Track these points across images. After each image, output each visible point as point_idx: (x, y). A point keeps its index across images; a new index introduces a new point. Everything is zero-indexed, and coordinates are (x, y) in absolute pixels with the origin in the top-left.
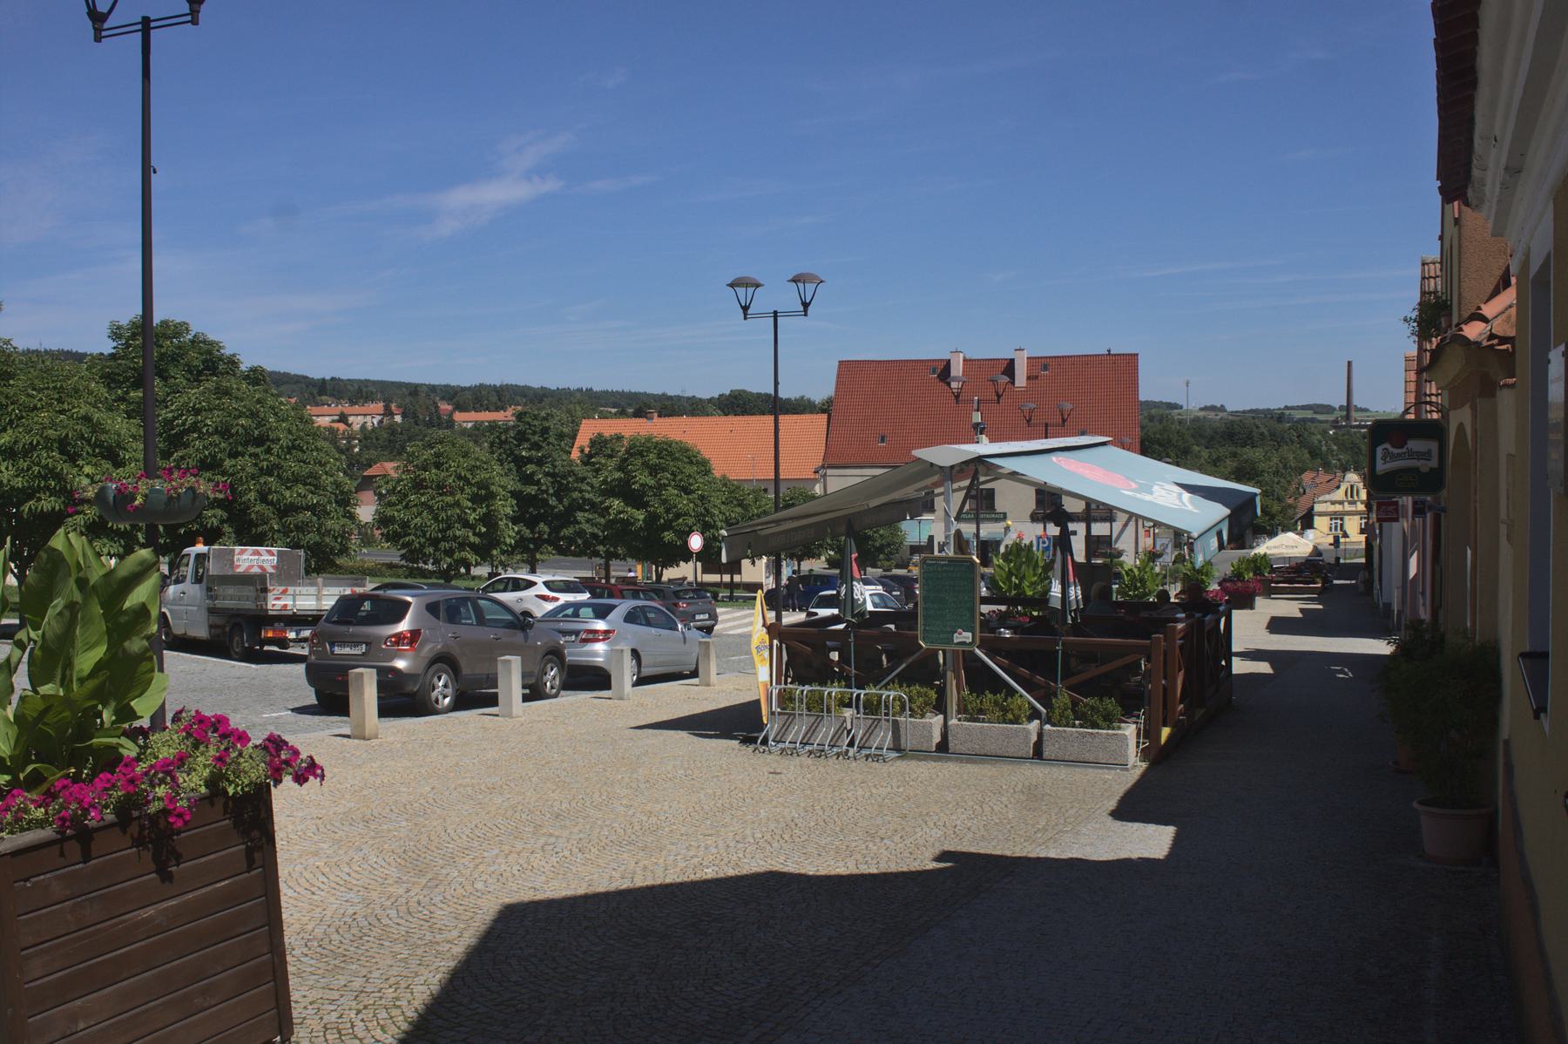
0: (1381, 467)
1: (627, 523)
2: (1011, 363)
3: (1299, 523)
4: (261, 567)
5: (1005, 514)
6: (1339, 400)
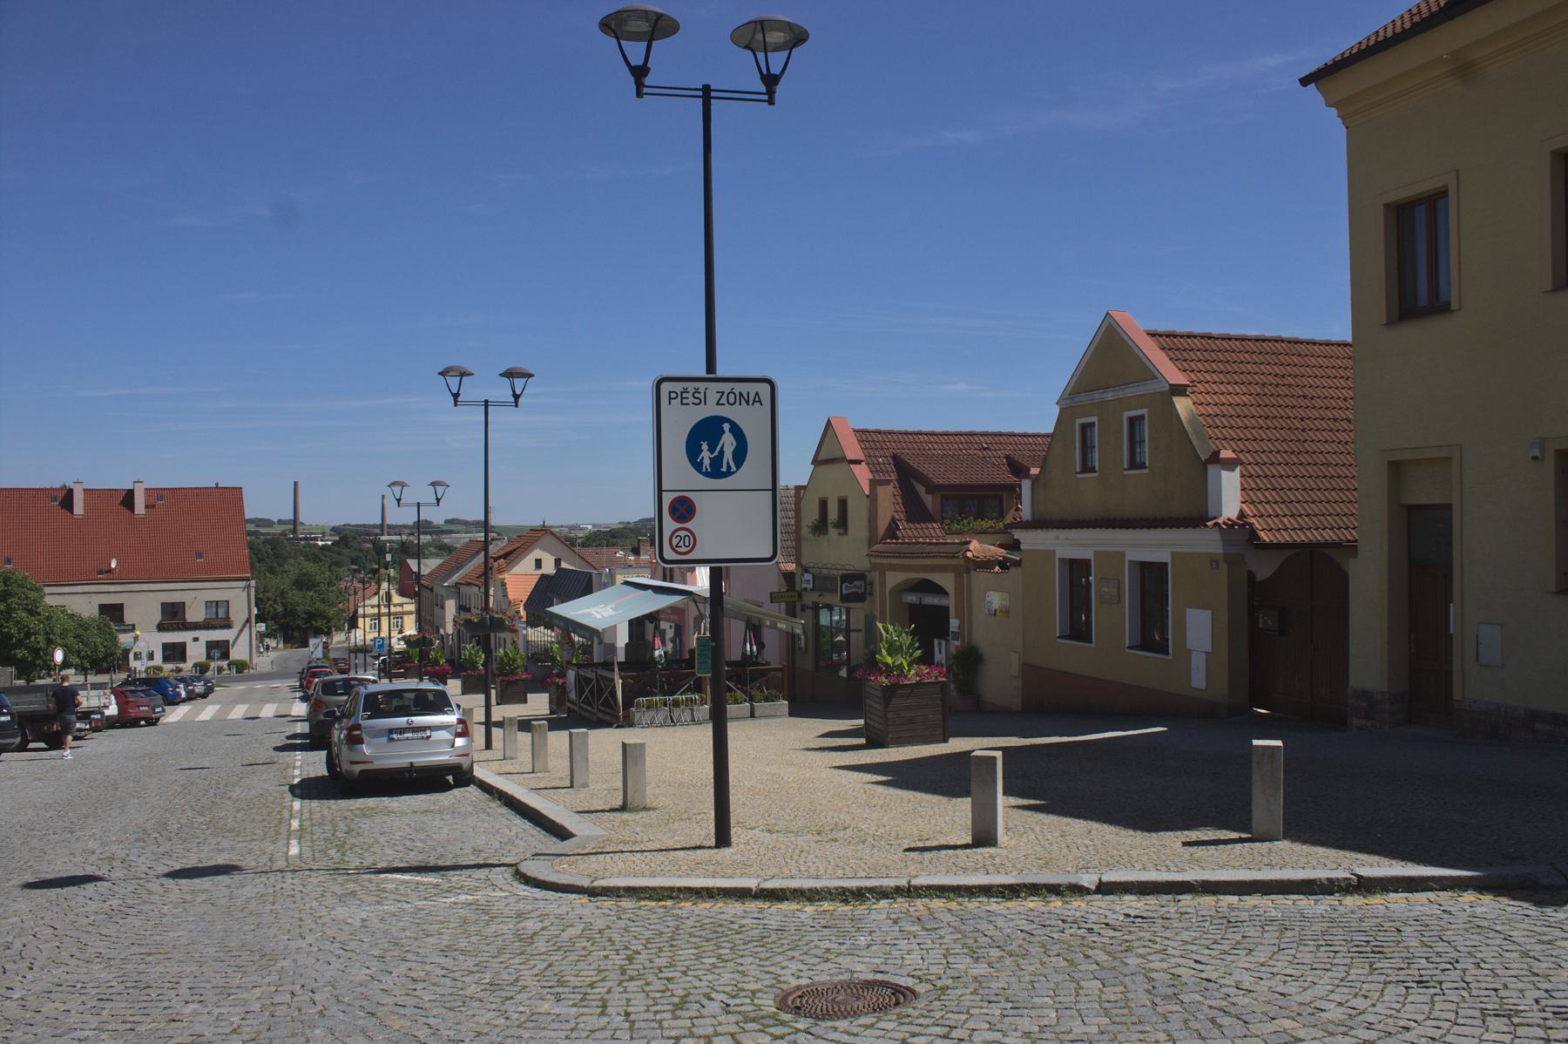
0: (844, 592)
2: (70, 492)
3: (346, 625)
5: (134, 625)
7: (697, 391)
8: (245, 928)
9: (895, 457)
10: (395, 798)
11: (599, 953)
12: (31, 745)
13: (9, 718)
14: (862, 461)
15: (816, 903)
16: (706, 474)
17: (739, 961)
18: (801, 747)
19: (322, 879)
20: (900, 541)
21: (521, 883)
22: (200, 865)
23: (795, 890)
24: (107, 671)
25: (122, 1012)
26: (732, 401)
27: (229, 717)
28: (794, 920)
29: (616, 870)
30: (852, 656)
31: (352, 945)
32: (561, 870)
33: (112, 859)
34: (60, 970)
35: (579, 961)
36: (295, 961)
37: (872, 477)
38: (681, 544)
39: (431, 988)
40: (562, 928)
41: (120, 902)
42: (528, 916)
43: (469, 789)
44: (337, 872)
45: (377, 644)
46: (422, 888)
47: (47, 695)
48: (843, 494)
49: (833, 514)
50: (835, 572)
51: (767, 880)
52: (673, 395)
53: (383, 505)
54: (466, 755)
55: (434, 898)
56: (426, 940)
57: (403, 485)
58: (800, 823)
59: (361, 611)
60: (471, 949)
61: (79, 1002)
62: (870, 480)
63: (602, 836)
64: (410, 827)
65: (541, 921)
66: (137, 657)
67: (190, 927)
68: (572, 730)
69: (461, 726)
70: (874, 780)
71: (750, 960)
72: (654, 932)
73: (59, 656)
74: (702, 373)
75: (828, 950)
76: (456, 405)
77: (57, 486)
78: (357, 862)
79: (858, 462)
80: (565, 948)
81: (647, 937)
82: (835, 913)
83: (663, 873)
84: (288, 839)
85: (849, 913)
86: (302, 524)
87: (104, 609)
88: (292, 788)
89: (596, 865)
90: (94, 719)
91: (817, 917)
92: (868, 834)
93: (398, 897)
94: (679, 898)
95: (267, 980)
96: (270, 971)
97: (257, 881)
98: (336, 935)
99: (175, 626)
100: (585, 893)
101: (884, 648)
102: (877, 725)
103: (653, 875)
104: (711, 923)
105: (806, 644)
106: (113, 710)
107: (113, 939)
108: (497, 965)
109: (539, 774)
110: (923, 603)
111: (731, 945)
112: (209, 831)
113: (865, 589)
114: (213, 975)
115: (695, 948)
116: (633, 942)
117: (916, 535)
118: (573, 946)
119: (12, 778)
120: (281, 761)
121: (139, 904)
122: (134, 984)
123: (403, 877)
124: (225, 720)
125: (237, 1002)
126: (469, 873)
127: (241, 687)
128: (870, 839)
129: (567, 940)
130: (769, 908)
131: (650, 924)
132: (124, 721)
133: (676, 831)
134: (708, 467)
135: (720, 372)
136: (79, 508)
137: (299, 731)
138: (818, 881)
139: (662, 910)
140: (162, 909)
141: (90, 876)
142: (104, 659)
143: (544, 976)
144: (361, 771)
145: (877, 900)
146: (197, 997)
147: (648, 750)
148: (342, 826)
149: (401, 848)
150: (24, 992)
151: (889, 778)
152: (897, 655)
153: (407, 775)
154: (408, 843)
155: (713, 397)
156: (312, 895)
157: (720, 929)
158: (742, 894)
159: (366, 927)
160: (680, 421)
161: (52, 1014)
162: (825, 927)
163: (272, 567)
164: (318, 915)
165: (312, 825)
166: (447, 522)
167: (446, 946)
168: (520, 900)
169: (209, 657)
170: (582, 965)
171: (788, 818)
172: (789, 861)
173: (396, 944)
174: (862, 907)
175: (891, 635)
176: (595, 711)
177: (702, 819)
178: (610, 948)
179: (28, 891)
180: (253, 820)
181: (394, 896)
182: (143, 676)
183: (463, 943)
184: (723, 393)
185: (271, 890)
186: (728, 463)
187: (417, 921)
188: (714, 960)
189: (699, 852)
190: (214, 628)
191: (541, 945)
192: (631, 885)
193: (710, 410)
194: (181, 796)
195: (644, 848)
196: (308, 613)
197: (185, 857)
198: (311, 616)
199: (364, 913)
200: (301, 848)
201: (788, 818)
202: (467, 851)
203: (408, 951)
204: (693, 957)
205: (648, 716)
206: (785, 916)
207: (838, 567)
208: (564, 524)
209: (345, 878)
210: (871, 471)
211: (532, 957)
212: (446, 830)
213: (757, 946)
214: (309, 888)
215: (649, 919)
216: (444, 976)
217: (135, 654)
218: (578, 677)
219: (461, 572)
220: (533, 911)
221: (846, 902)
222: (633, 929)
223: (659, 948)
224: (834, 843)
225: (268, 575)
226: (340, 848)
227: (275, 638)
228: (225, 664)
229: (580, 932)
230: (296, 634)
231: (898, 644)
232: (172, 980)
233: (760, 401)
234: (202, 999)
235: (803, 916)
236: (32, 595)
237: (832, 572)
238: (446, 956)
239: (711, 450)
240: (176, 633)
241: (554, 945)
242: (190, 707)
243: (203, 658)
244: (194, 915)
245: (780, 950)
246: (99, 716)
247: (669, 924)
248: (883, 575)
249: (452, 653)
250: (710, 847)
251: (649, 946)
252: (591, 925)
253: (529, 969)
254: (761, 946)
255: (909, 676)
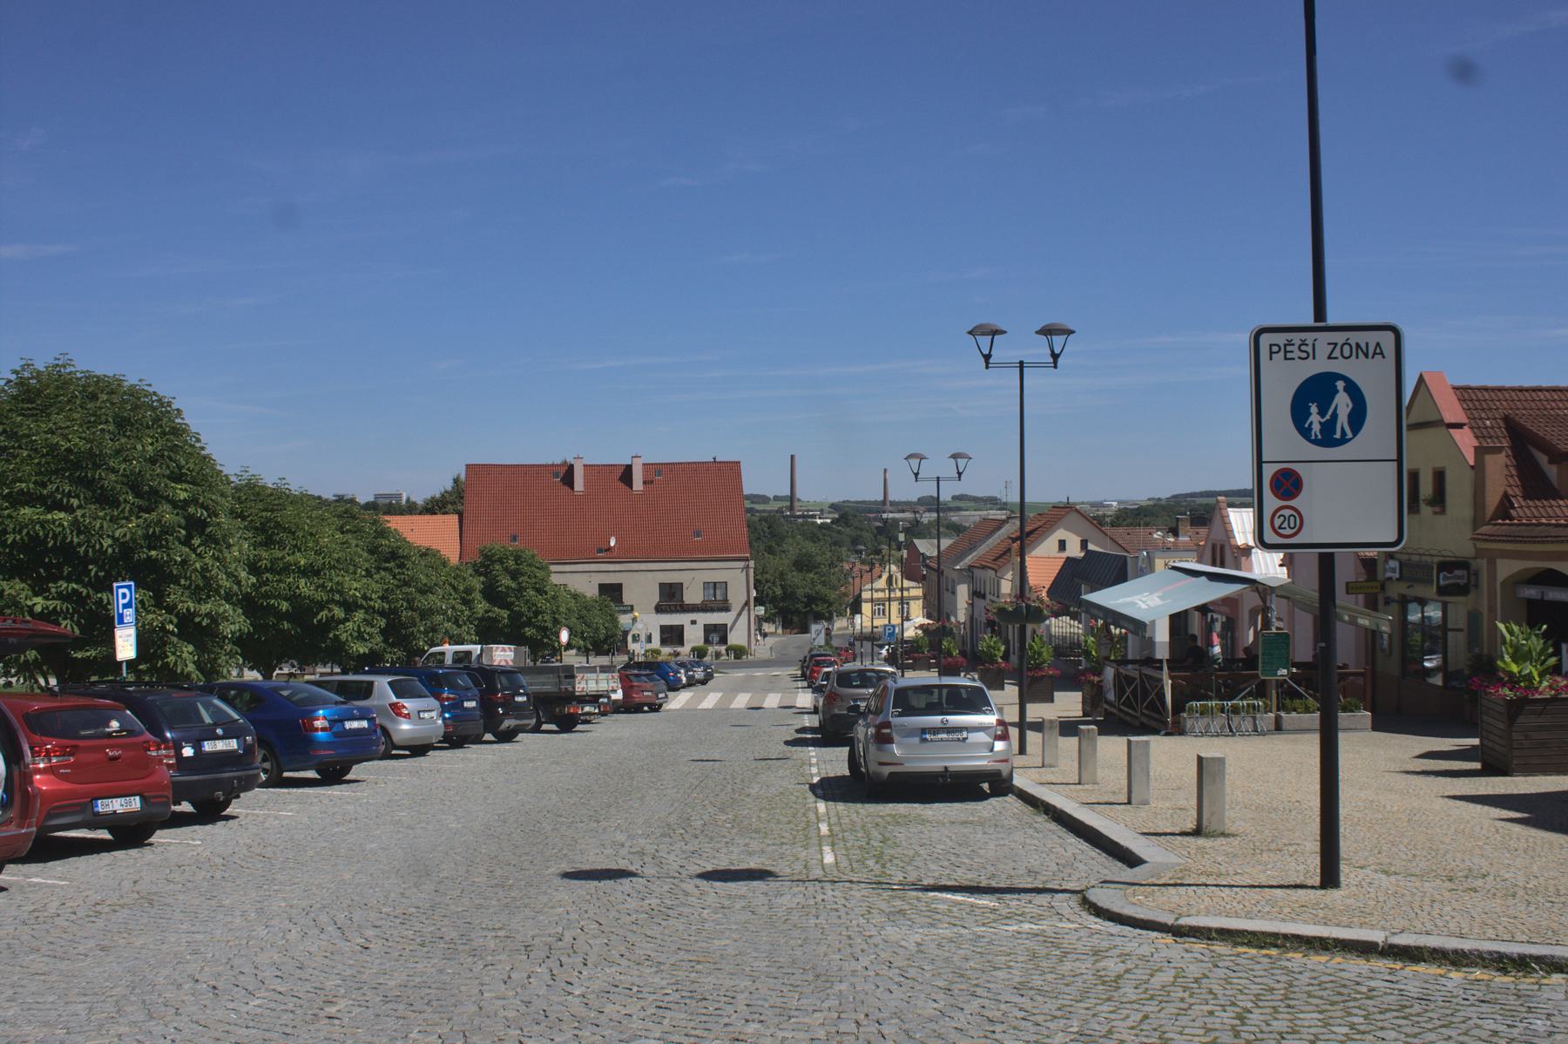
0: (1442, 582)
1: (496, 620)
4: (506, 661)
5: (632, 606)
6: (881, 498)
7: (1304, 343)
8: (792, 942)
9: (1506, 419)
10: (927, 806)
11: (1202, 1007)
12: (545, 727)
13: (525, 699)
14: (1465, 424)
15: (1464, 969)
16: (1316, 442)
17: (1379, 1034)
18: (1397, 770)
19: (864, 892)
20: (1516, 521)
21: (1091, 914)
22: (732, 868)
23: (1435, 951)
24: (606, 653)
25: (683, 1023)
26: (1347, 353)
27: (732, 706)
28: (1438, 987)
29: (1202, 906)
30: (1449, 660)
31: (912, 973)
32: (1138, 902)
33: (642, 853)
34: (613, 969)
35: (1178, 1015)
36: (853, 985)
37: (1477, 444)
38: (1285, 525)
39: (1012, 1031)
40: (1149, 972)
41: (658, 901)
42: (1107, 954)
43: (1006, 798)
44: (879, 886)
45: (887, 632)
46: (978, 912)
47: (559, 677)
48: (1438, 465)
49: (1426, 489)
50: (1429, 559)
51: (1394, 934)
52: (1275, 349)
53: (885, 480)
54: (1006, 761)
55: (994, 925)
56: (994, 973)
57: (922, 458)
58: (1423, 865)
59: (866, 595)
60: (1049, 989)
61: (639, 1006)
62: (1476, 448)
63: (1179, 864)
64: (951, 840)
65: (1123, 962)
66: (636, 639)
67: (735, 936)
68: (1132, 738)
69: (1000, 728)
70: (1505, 817)
71: (1393, 1034)
72: (1261, 986)
73: (564, 636)
74: (1309, 320)
75: (1495, 1033)
76: (987, 367)
77: (558, 461)
78: (899, 877)
79: (1459, 426)
80: (1160, 998)
81: (1256, 992)
82: (1492, 985)
83: (1260, 915)
84: (820, 845)
85: (1512, 987)
86: (799, 500)
87: (604, 588)
88: (813, 787)
89: (1176, 899)
90: (603, 703)
91: (1468, 987)
92: (1516, 885)
93: (953, 921)
94: (1285, 946)
95: (826, 1005)
96: (828, 995)
97: (796, 890)
98: (892, 960)
99: (673, 608)
100: (1168, 932)
101: (1508, 654)
102: (1497, 748)
103: (1249, 916)
104: (1332, 982)
105: (1390, 644)
106: (619, 695)
107: (659, 942)
108: (1084, 1011)
109: (1086, 786)
110: (1546, 598)
111: (1364, 1013)
112: (735, 831)
113: (1469, 580)
114: (768, 993)
115: (1319, 1012)
116: (1240, 997)
117: (1536, 514)
118: (1168, 995)
119: (531, 760)
120: (795, 757)
121: (678, 906)
122: (689, 994)
123: (954, 897)
124: (728, 709)
125: (800, 1026)
126: (1028, 898)
127: (740, 674)
128: (1521, 893)
129: (1159, 987)
130: (1401, 969)
131: (1255, 977)
132: (629, 707)
133: (1266, 864)
134: (1318, 433)
135: (1332, 319)
136: (579, 484)
137: (808, 725)
138: (1463, 940)
139: (1266, 960)
140: (701, 913)
141: (624, 871)
142: (605, 642)
143: (1142, 1030)
144: (890, 773)
145: (1547, 972)
146: (758, 1015)
147: (1229, 769)
148: (875, 833)
149: (946, 864)
150: (583, 989)
151: (1526, 815)
152: (1525, 662)
153: (941, 780)
154: (953, 858)
155: (1323, 350)
156: (857, 910)
157: (1345, 991)
158: (1365, 949)
159: (922, 952)
160: (1284, 380)
161: (615, 1016)
162: (1483, 1001)
163: (770, 547)
164: (868, 933)
165: (844, 831)
166: (955, 498)
167: (1020, 983)
168: (1092, 934)
169: (707, 641)
170: (1183, 1021)
171: (1405, 857)
172: (1419, 912)
173: (962, 976)
174: (1528, 980)
175: (1517, 638)
176: (1138, 714)
177: (1296, 851)
178: (1212, 1002)
179: (567, 880)
180: (779, 822)
181: (948, 919)
182: (641, 659)
183: (1037, 982)
184: (1336, 344)
185: (812, 902)
186: (1342, 428)
187: (979, 950)
188: (1345, 1030)
189: (1301, 892)
190: (712, 610)
191: (1129, 991)
192: (1225, 926)
193: (1320, 365)
194: (698, 790)
195: (1232, 883)
196: (808, 596)
197: (714, 857)
198: (811, 599)
199: (917, 936)
200: (836, 856)
201: (1405, 857)
202: (1021, 872)
203: (977, 985)
204: (1320, 1024)
205: (1200, 724)
206: (1426, 982)
207: (1432, 552)
208: (1085, 501)
209: (890, 893)
210: (1477, 437)
211: (1122, 1006)
212: (992, 846)
213: (1397, 1017)
214: (853, 902)
215: (1252, 970)
216: (1023, 1019)
217: (634, 636)
218: (1117, 675)
219: (974, 554)
220: (1110, 948)
221: (1504, 971)
222: (1235, 981)
223: (1274, 1007)
224: (1473, 894)
225: (766, 555)
226: (879, 858)
227: (774, 622)
228: (723, 649)
229: (1172, 979)
230: (795, 619)
231: (1526, 648)
232: (728, 993)
233: (1382, 353)
234: (762, 1018)
235: (1450, 985)
236: (540, 574)
237: (1424, 558)
238: (1022, 995)
239: (1322, 413)
240: (674, 615)
241: (1145, 993)
242: (692, 694)
243: (701, 643)
244: (736, 923)
245: (1430, 1026)
246: (606, 700)
247: (1278, 978)
248: (1492, 564)
249: (964, 643)
250: (1313, 887)
251: (1261, 1004)
252: (1184, 971)
253: (1122, 1020)
254: (1404, 1018)
255: (1541, 689)
